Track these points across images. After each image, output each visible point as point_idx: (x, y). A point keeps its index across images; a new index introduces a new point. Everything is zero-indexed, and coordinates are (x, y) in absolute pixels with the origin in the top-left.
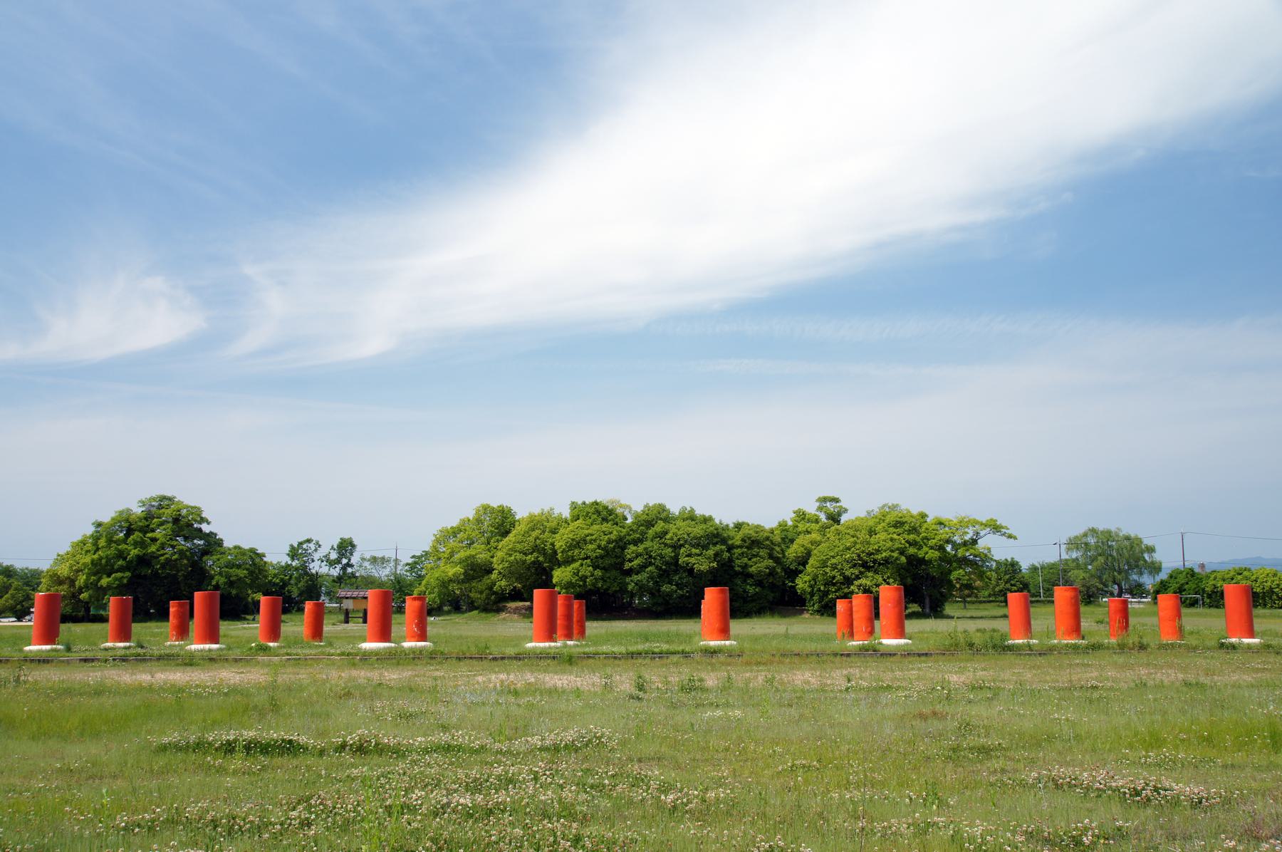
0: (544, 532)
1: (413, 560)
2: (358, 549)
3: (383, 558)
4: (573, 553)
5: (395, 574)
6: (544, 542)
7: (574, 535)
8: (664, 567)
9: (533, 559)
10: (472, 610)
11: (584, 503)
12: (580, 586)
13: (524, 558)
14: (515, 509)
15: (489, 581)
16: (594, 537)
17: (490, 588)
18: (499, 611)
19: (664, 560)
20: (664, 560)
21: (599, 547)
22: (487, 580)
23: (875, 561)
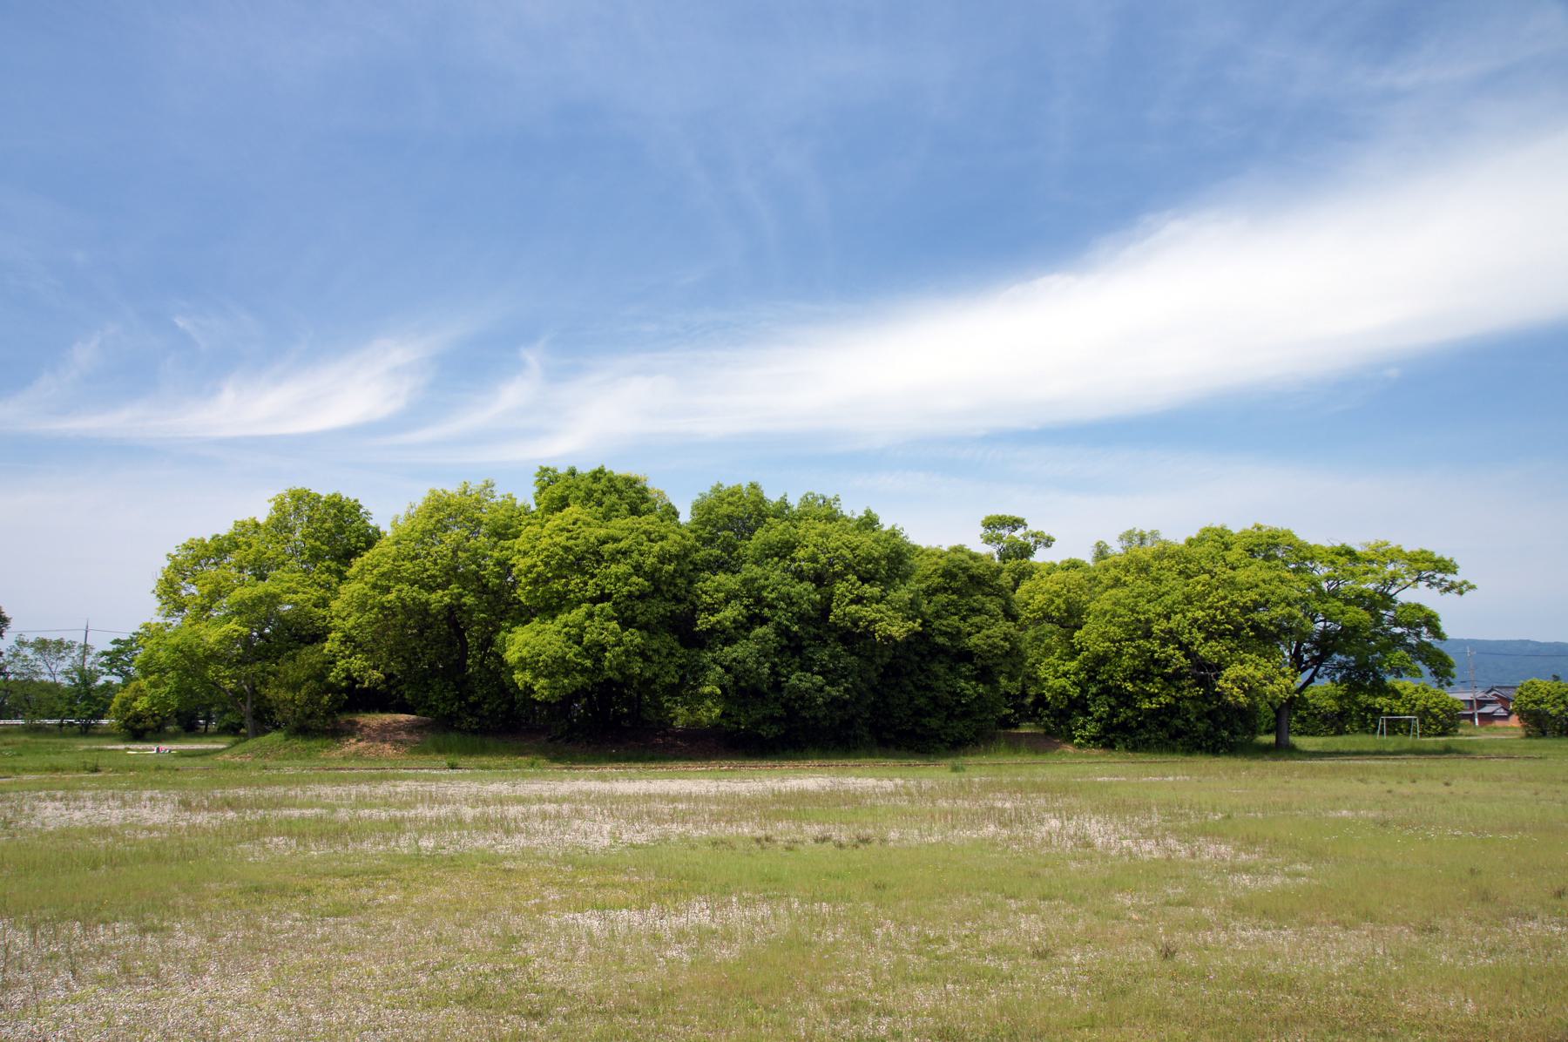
0: (474, 533)
1: (115, 646)
2: (13, 625)
3: (60, 643)
4: (566, 585)
5: (81, 672)
6: (475, 556)
7: (568, 539)
8: (795, 628)
9: (447, 600)
10: (266, 732)
11: (573, 473)
12: (584, 670)
13: (424, 596)
14: (367, 505)
15: (314, 659)
16: (623, 545)
17: (320, 676)
18: (337, 733)
19: (796, 609)
20: (796, 609)
21: (638, 569)
22: (309, 656)
23: (1255, 627)
